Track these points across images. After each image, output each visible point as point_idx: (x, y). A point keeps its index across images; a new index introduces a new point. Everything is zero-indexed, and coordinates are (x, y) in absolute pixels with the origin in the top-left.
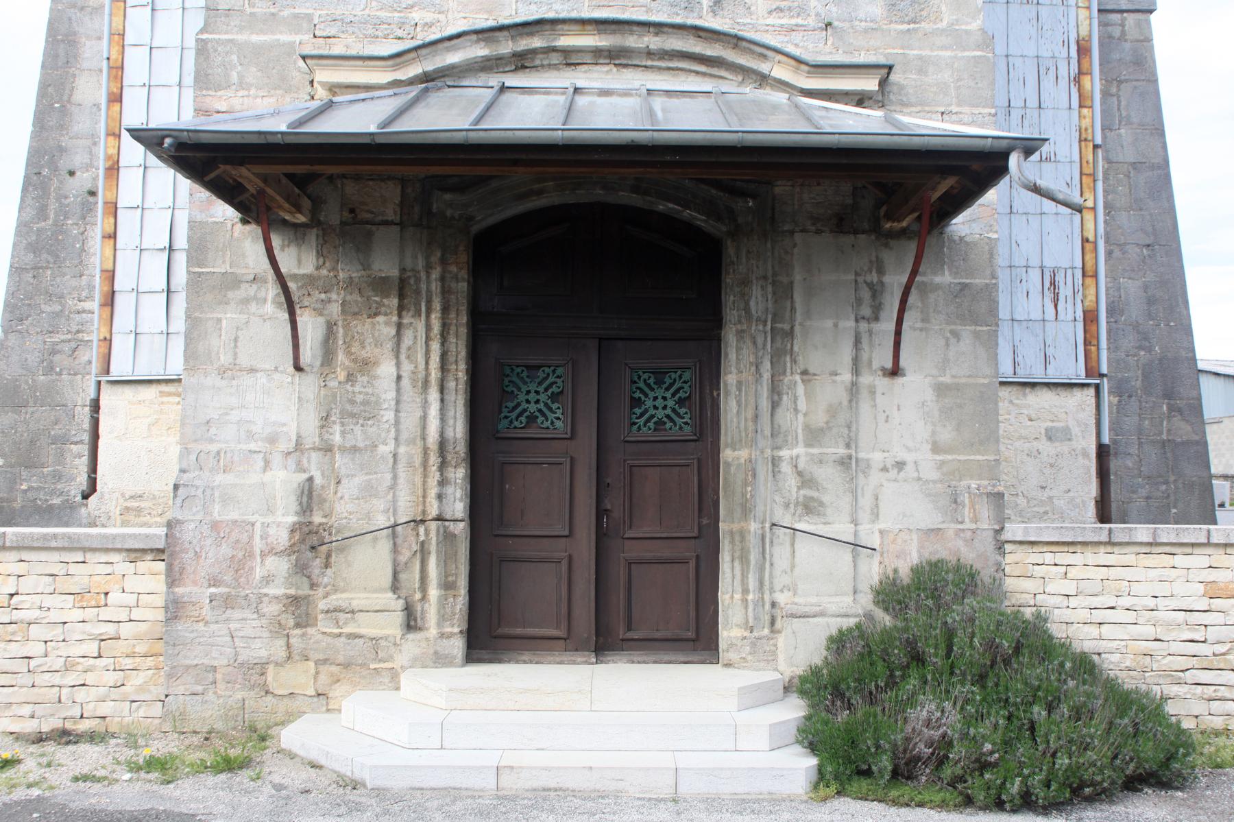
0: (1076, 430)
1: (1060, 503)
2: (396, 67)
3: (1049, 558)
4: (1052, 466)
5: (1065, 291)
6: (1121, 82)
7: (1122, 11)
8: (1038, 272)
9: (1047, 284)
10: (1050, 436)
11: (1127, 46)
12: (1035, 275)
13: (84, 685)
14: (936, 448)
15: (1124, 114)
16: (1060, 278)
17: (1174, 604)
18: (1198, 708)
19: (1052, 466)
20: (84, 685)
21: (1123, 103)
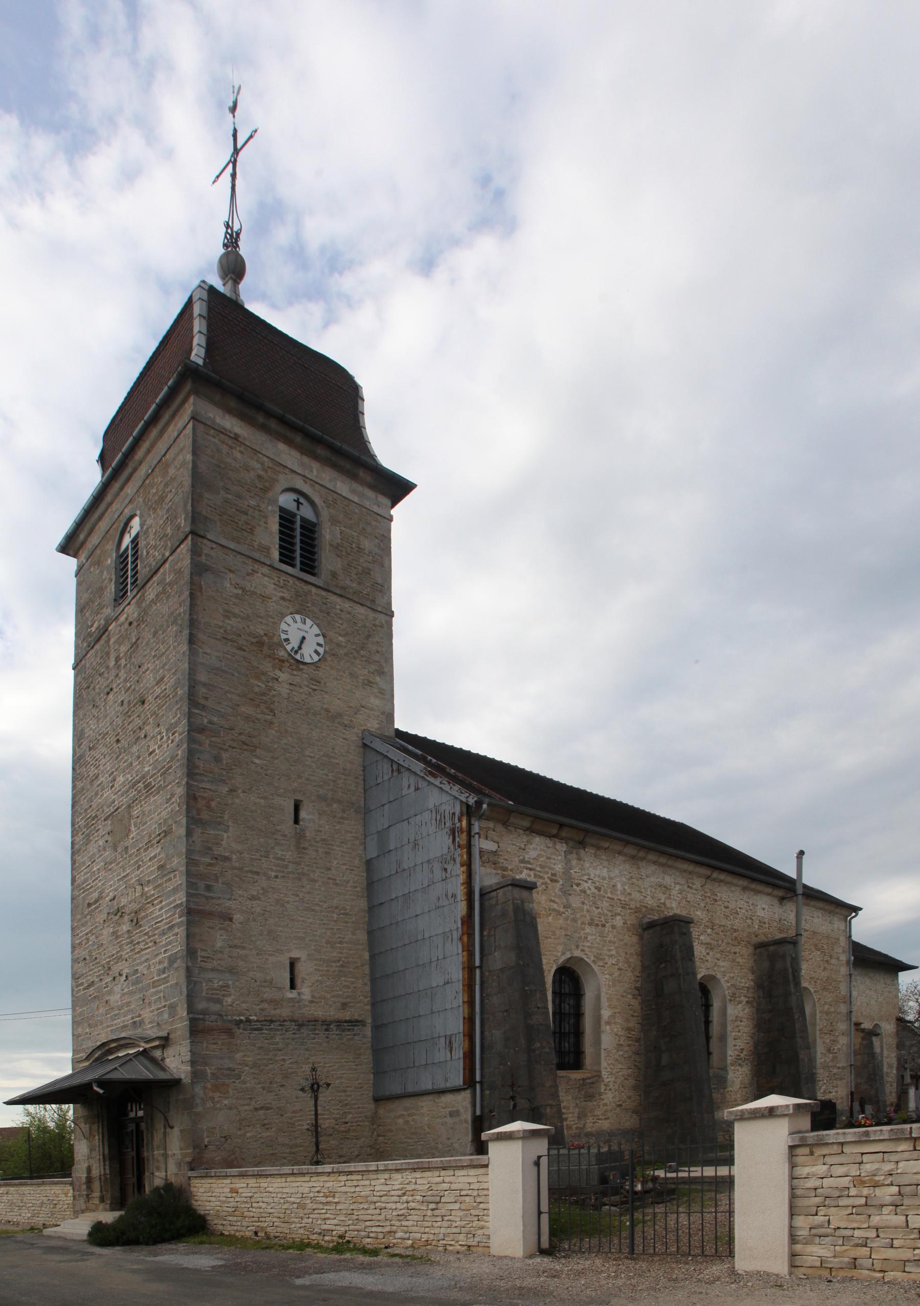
0: (462, 1111)
1: (456, 1145)
2: (89, 1060)
3: (199, 1181)
4: (452, 1128)
5: (455, 1045)
6: (496, 928)
7: (496, 890)
8: (444, 1038)
9: (448, 1043)
10: (451, 1114)
11: (499, 907)
12: (442, 1040)
13: (822, 1178)
14: (181, 1149)
15: (497, 944)
16: (453, 1039)
17: (224, 1195)
18: (229, 1228)
19: (452, 1128)
20: (822, 1178)
21: (497, 939)
